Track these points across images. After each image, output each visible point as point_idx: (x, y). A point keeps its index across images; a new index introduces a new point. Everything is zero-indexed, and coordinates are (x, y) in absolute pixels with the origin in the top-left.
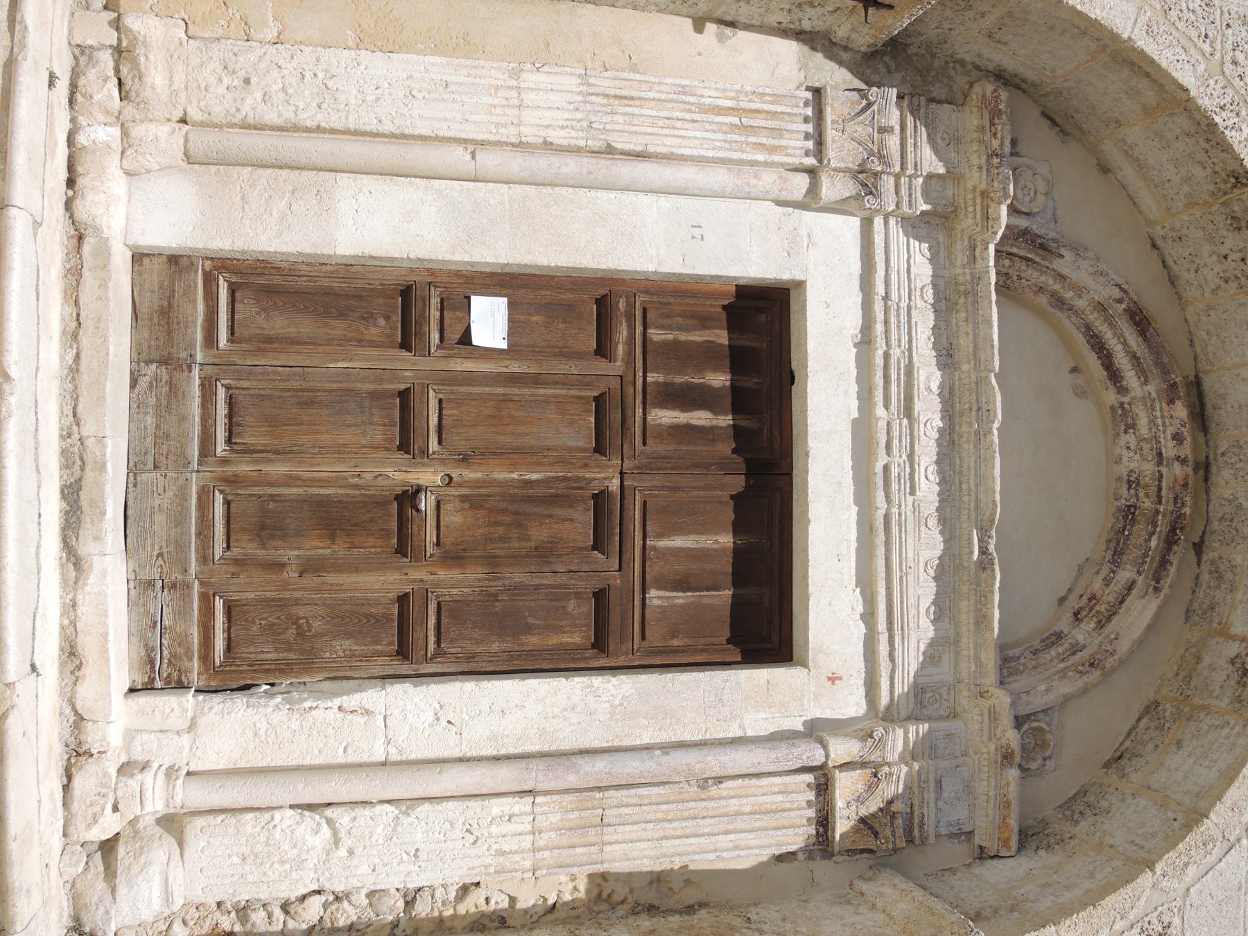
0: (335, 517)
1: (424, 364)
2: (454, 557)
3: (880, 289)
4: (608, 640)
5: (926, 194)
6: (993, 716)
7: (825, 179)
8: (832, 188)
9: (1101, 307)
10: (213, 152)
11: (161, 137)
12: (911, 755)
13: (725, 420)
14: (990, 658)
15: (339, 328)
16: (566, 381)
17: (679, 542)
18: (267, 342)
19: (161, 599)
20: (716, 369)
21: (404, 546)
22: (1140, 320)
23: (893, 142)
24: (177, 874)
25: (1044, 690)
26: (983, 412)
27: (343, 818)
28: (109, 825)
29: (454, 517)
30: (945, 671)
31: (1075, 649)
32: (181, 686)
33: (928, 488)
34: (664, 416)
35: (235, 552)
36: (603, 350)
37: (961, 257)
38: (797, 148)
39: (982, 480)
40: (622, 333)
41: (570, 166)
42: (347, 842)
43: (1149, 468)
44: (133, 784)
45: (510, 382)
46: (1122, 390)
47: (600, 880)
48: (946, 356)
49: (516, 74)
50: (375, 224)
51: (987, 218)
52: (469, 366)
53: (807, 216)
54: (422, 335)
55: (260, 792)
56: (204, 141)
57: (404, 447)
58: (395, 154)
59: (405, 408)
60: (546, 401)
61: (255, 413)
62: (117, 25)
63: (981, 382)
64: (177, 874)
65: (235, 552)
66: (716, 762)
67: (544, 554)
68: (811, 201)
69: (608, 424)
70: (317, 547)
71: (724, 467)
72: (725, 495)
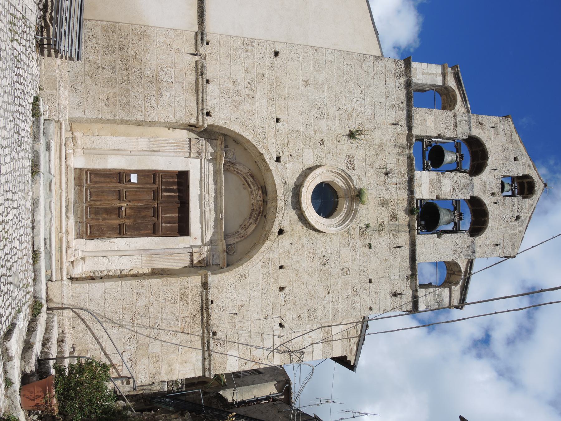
0: (108, 211)
1: (123, 186)
2: (128, 218)
3: (203, 172)
4: (155, 232)
5: (211, 155)
6: (223, 244)
7: (192, 154)
9: (245, 174)
10: (87, 152)
11: (79, 151)
12: (208, 251)
13: (177, 194)
14: (223, 235)
15: (108, 180)
16: (148, 188)
17: (168, 215)
18: (96, 182)
19: (80, 225)
20: (175, 185)
21: (120, 216)
24: (84, 266)
25: (232, 241)
26: (221, 193)
27: (110, 258)
28: (73, 259)
30: (216, 237)
31: (241, 233)
32: (82, 238)
33: (212, 205)
34: (166, 194)
35: (91, 217)
36: (154, 183)
37: (218, 166)
38: (187, 148)
39: (221, 204)
40: (158, 179)
41: (147, 153)
42: (111, 262)
43: (256, 202)
44: (77, 252)
46: (251, 188)
47: (153, 270)
48: (215, 183)
49: (137, 139)
50: (114, 163)
51: (221, 160)
52: (130, 186)
53: (190, 159)
54: (122, 181)
55: (97, 254)
57: (119, 199)
58: (117, 152)
59: (119, 193)
60: (144, 191)
61: (94, 194)
62: (72, 134)
63: (221, 187)
64: (84, 266)
65: (91, 217)
66: (172, 251)
67: (144, 217)
68: (190, 157)
70: (105, 216)
71: (176, 202)
72: (177, 207)
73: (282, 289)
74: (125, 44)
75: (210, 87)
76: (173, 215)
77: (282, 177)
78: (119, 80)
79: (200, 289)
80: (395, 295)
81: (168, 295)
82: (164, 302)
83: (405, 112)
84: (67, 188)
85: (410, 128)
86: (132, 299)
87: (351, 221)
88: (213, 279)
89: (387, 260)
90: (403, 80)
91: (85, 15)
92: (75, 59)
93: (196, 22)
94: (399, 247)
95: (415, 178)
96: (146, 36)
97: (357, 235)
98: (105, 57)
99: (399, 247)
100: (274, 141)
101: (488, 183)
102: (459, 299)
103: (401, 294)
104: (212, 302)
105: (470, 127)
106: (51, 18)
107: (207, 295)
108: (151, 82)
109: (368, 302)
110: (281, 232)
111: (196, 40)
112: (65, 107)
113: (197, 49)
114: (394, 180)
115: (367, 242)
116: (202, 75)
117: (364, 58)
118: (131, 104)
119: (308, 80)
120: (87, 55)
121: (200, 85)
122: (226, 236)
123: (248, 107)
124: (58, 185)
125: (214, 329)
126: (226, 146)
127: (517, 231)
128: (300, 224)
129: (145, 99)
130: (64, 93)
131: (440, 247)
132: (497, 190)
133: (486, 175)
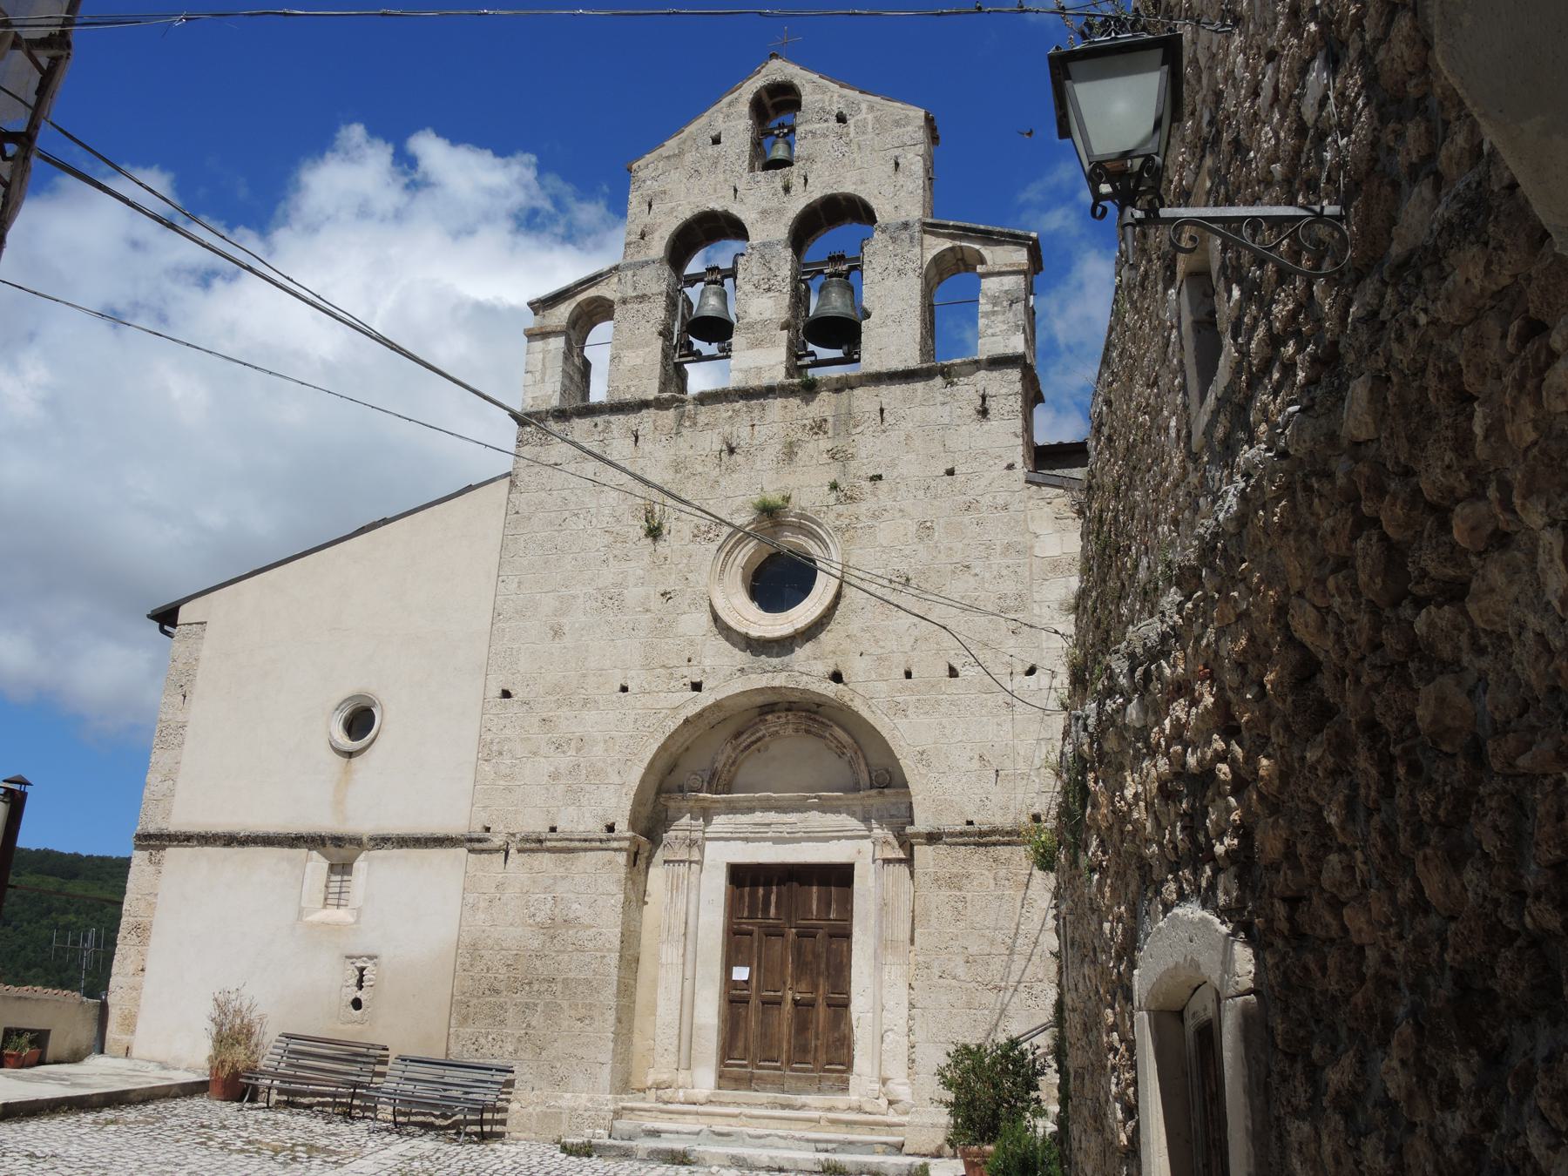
0: (802, 1026)
2: (815, 988)
4: (844, 934)
8: (696, 856)
10: (687, 1062)
11: (682, 1077)
14: (851, 796)
15: (742, 1024)
17: (815, 907)
18: (746, 1049)
21: (811, 1004)
22: (738, 735)
23: (680, 834)
25: (864, 778)
26: (768, 799)
28: (883, 1102)
29: (803, 986)
30: (858, 809)
36: (750, 934)
38: (683, 869)
39: (790, 799)
41: (690, 948)
45: (763, 969)
48: (751, 810)
50: (709, 1011)
51: (704, 799)
56: (683, 1064)
58: (687, 1004)
63: (759, 799)
68: (700, 863)
69: (774, 932)
70: (811, 1034)
73: (953, 673)
74: (489, 984)
75: (561, 826)
76: (815, 896)
77: (731, 677)
78: (548, 997)
79: (942, 849)
80: (984, 413)
81: (948, 914)
82: (962, 925)
83: (613, 418)
84: (748, 1104)
85: (644, 405)
86: (952, 988)
87: (820, 525)
88: (923, 822)
89: (908, 437)
90: (553, 426)
91: (439, 1055)
92: (509, 1076)
93: (452, 851)
94: (882, 411)
95: (742, 384)
96: (474, 946)
97: (852, 508)
98: (509, 1022)
99: (882, 411)
100: (662, 695)
101: (764, 204)
102: (1011, 248)
103: (984, 398)
104: (970, 823)
105: (647, 263)
106: (444, 1116)
107: (951, 835)
108: (553, 938)
109: (995, 474)
110: (837, 677)
111: (482, 851)
112: (591, 1100)
113: (498, 851)
114: (745, 432)
115: (867, 485)
116: (540, 841)
117: (513, 514)
118: (590, 977)
119: (552, 628)
120: (506, 1055)
121: (559, 844)
122: (856, 788)
123: (599, 750)
124: (732, 1121)
125: (1025, 819)
126: (681, 789)
127: (870, 117)
128: (822, 636)
129: (581, 950)
130: (567, 1100)
131: (890, 311)
132: (777, 178)
133: (745, 213)
